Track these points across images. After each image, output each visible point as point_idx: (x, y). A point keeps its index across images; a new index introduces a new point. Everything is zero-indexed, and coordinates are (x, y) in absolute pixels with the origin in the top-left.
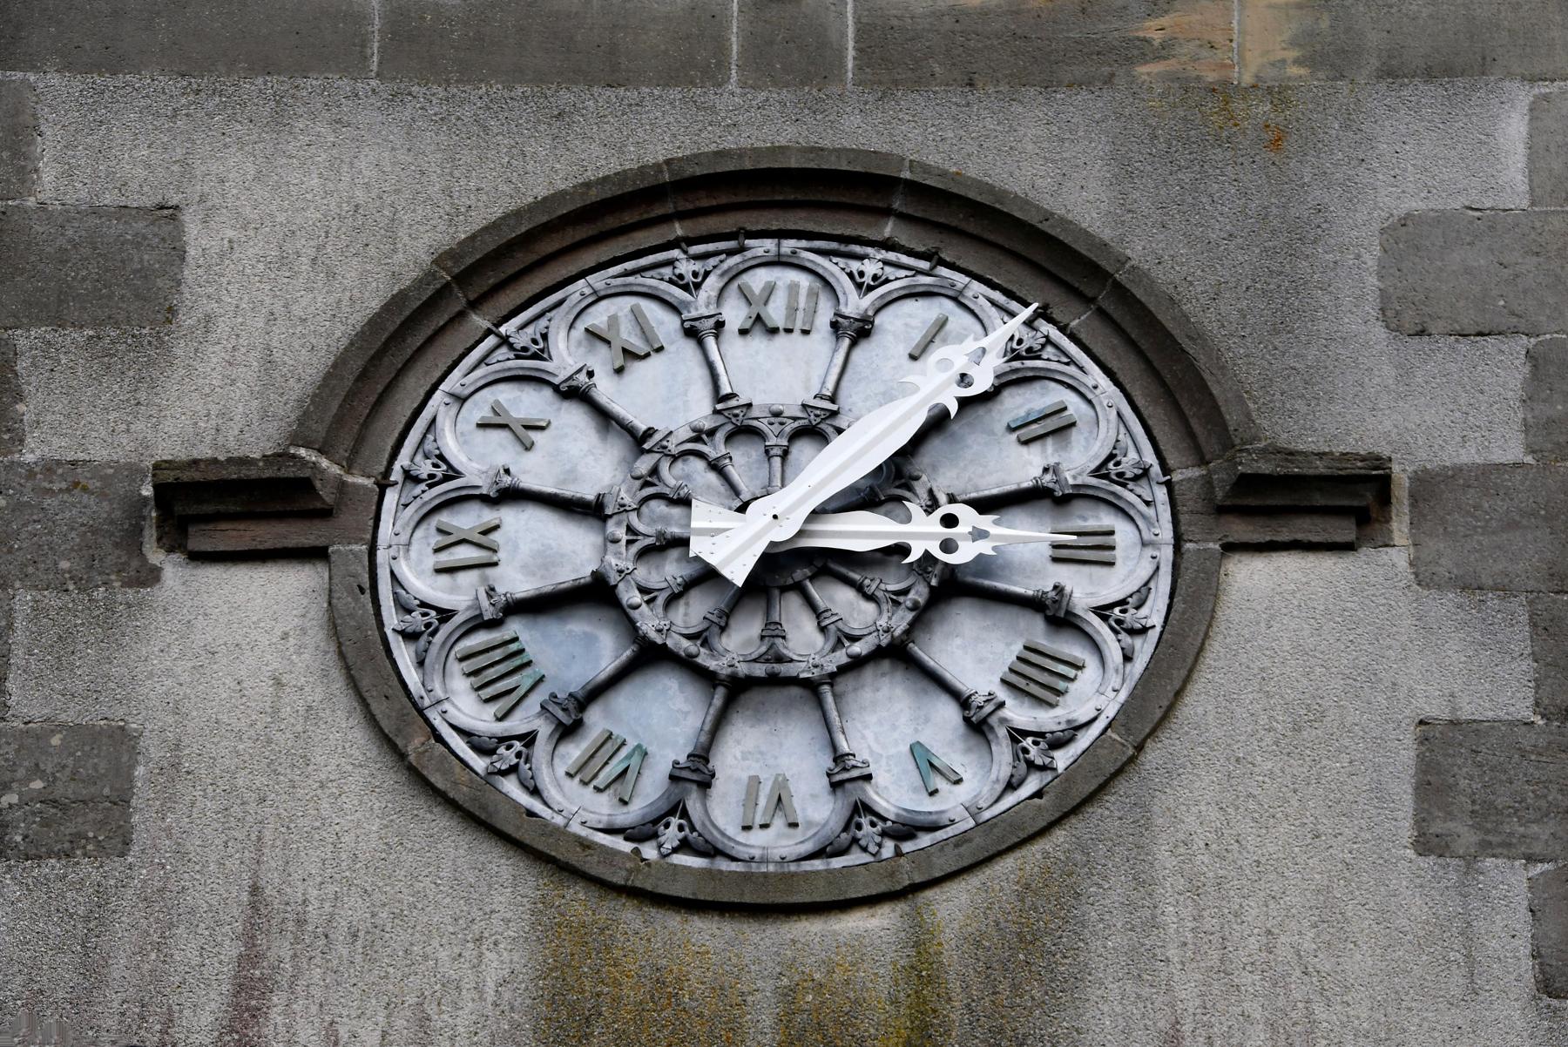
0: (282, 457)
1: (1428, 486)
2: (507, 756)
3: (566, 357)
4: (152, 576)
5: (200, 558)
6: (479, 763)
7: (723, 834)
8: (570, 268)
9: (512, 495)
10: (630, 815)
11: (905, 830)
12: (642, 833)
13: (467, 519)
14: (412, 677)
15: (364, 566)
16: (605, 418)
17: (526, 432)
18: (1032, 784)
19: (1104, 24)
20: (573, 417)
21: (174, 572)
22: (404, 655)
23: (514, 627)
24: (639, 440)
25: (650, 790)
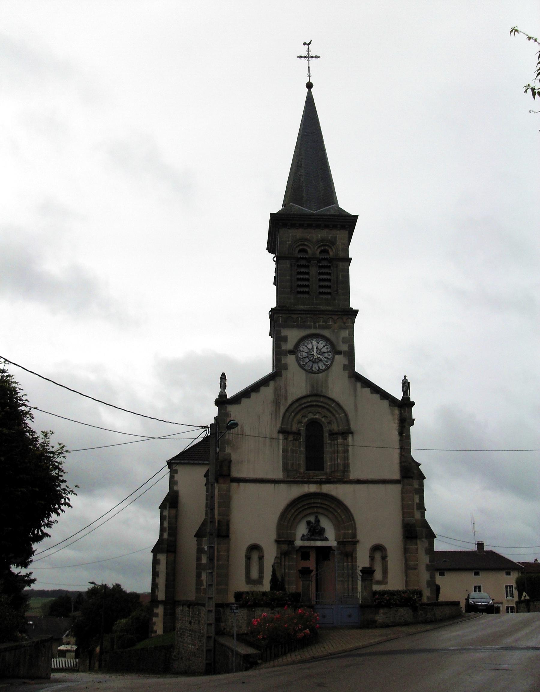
0: (293, 350)
1: (344, 351)
2: (304, 365)
3: (306, 344)
4: (288, 356)
5: (290, 355)
6: (302, 366)
7: (312, 590)
8: (320, 404)
9: (303, 352)
10: (309, 369)
11: (321, 369)
12: (310, 369)
13: (301, 353)
14: (299, 361)
15: (525, 624)
16: (307, 348)
17: (304, 348)
18: (327, 367)
19: (233, 626)
20: (306, 347)
21: (288, 355)
22: (299, 360)
23: (304, 359)
24: (309, 349)
25: (310, 367)
